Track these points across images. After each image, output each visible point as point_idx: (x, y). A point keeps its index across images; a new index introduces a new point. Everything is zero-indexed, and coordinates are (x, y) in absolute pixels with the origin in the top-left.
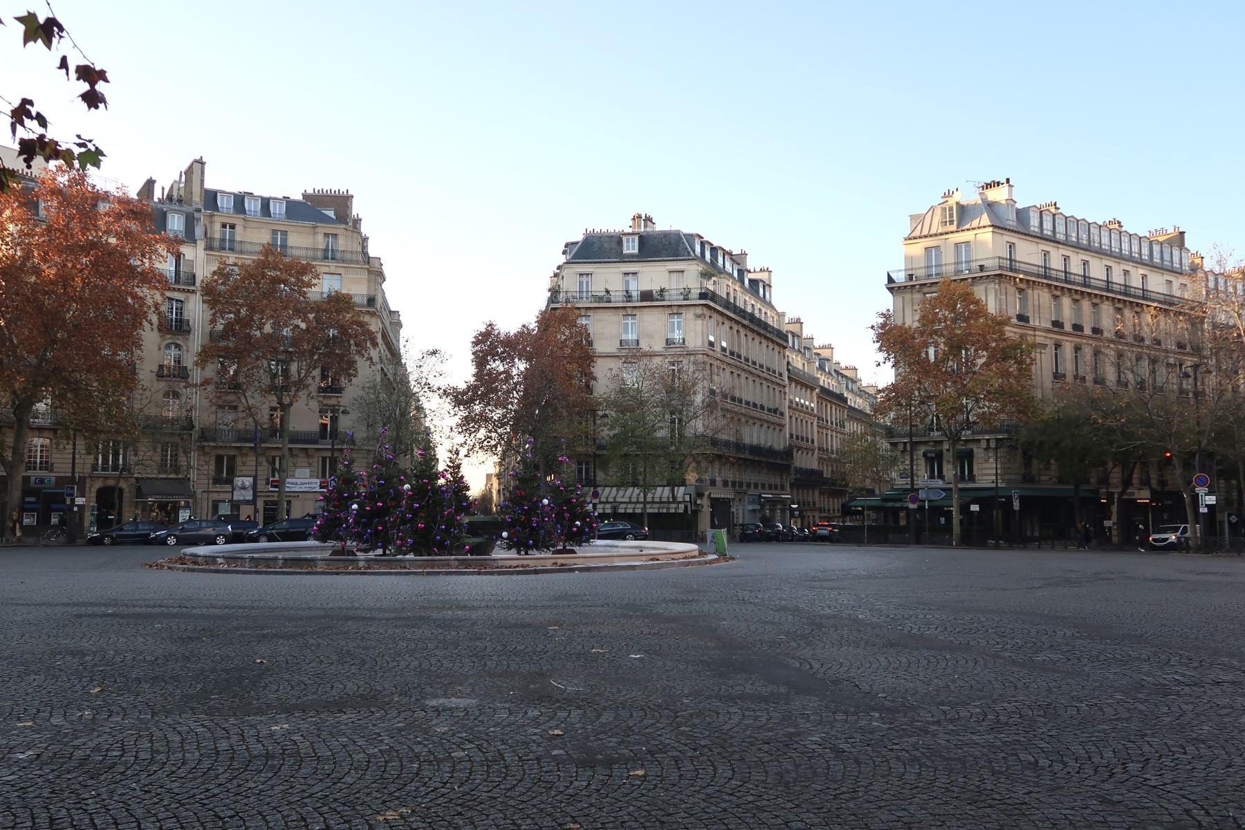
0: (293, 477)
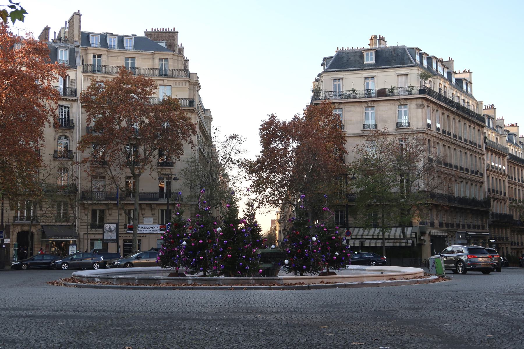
0: (142, 223)
